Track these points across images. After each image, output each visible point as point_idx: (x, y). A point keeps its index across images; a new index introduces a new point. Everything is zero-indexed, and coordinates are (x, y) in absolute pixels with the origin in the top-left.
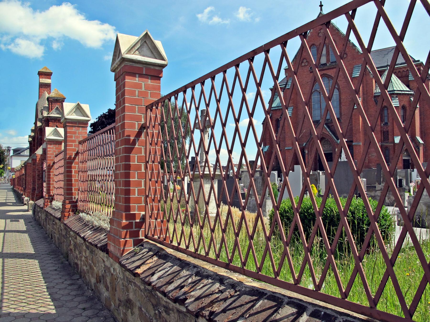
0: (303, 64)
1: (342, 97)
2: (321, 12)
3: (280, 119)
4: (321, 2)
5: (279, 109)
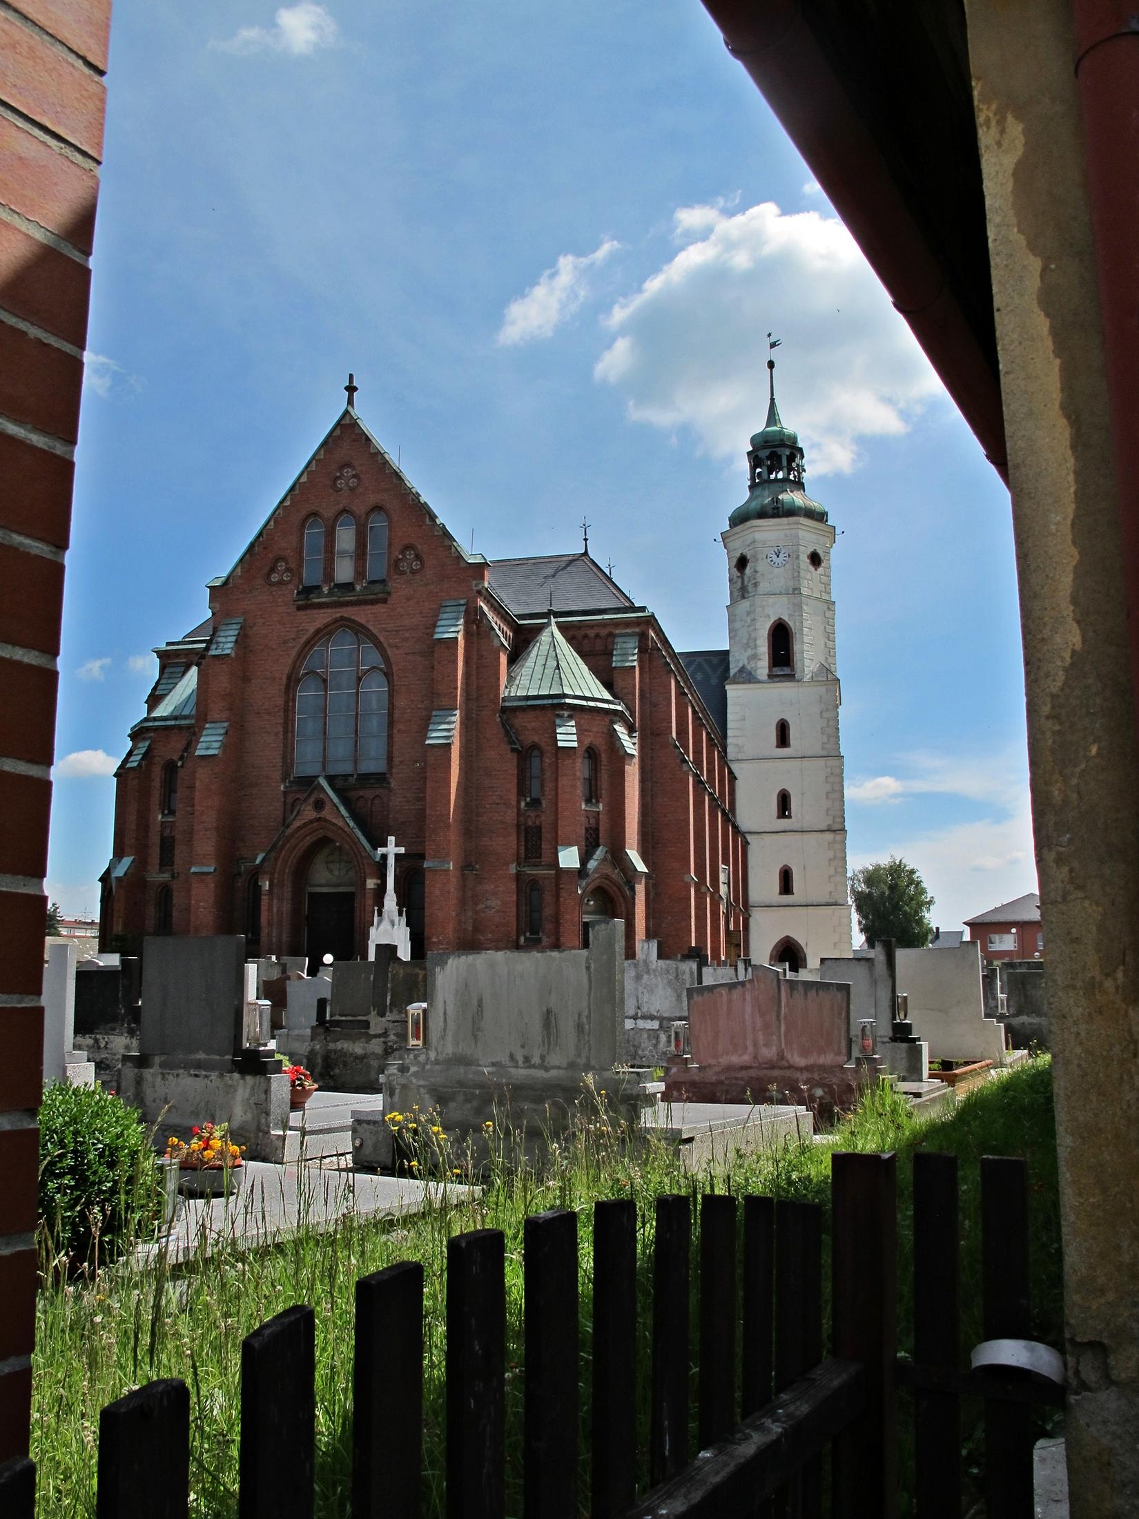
0: (275, 578)
2: (350, 409)
3: (180, 764)
4: (351, 376)
5: (180, 728)
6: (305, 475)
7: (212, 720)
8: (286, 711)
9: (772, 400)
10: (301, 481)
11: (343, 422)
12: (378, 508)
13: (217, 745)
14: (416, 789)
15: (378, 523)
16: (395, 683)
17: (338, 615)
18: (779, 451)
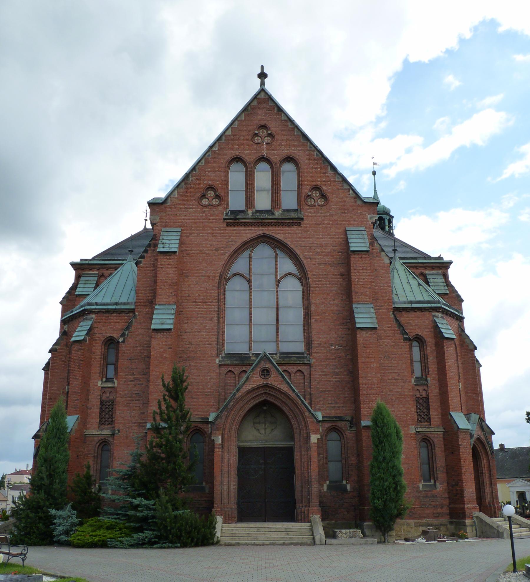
0: (205, 202)
1: (313, 301)
3: (121, 340)
4: (262, 67)
6: (230, 129)
7: (160, 303)
8: (219, 301)
9: (375, 191)
10: (227, 133)
11: (259, 97)
12: (289, 159)
13: (172, 321)
15: (288, 169)
16: (311, 285)
17: (261, 232)
18: (384, 216)
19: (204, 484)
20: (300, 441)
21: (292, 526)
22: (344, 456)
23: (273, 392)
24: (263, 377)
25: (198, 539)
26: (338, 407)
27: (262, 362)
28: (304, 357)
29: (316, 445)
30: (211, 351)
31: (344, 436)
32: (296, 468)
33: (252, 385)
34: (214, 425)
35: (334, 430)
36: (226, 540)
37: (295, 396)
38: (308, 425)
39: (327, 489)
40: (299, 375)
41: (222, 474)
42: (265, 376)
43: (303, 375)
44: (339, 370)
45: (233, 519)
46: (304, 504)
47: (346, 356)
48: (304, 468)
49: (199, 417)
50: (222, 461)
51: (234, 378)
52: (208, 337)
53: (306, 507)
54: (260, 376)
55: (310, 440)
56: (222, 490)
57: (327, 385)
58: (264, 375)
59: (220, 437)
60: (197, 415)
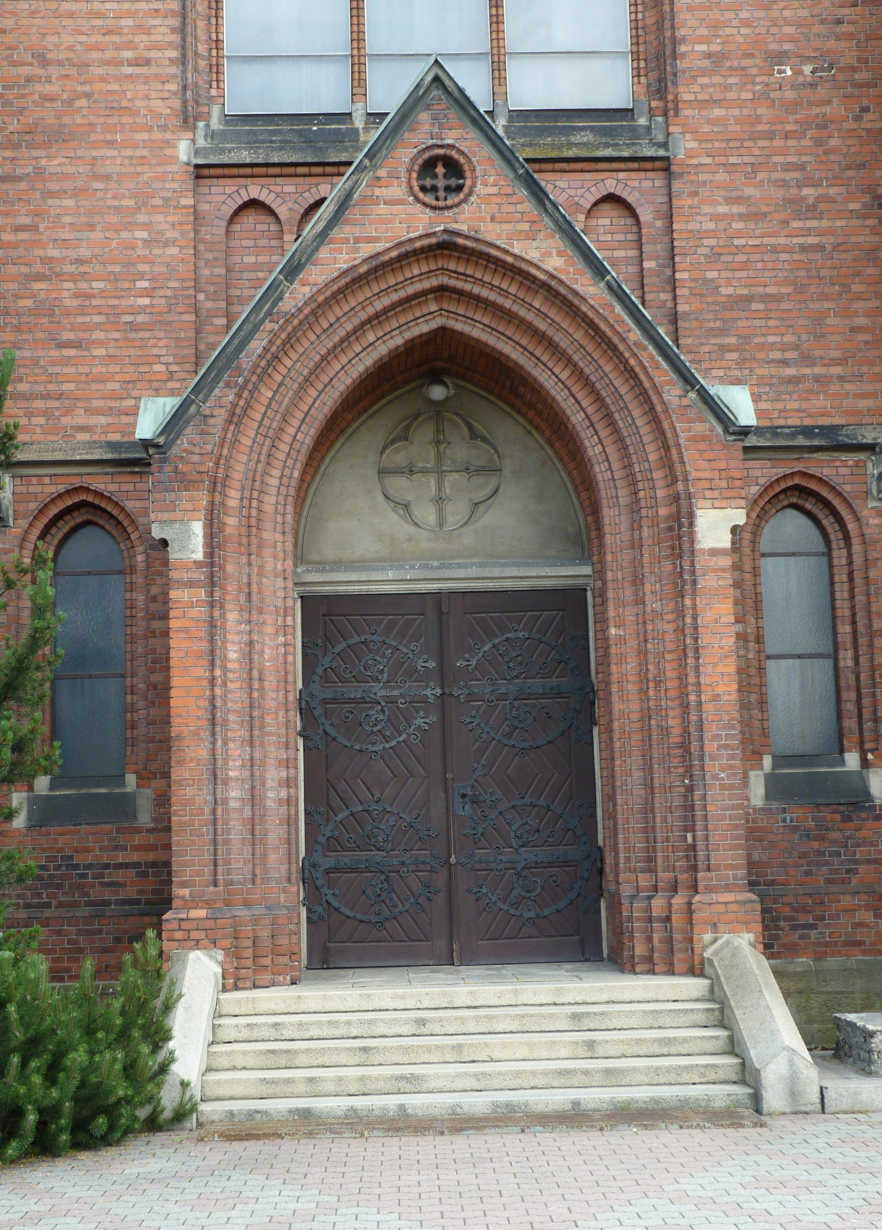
14: (788, 167)
19: (131, 779)
20: (636, 544)
21: (605, 998)
22: (848, 628)
23: (483, 284)
24: (429, 199)
25: (48, 1115)
26: (817, 379)
27: (424, 116)
28: (634, 133)
29: (726, 562)
30: (147, 97)
31: (851, 527)
32: (614, 688)
33: (371, 240)
34: (164, 461)
35: (794, 500)
36: (238, 1091)
37: (608, 297)
38: (680, 453)
39: (768, 796)
40: (607, 221)
41: (213, 722)
42: (441, 194)
43: (630, 221)
44: (821, 191)
45: (285, 960)
46: (664, 876)
47: (857, 118)
48: (658, 683)
49: (96, 438)
50: (212, 652)
51: (274, 243)
52: (129, 22)
53: (675, 891)
54: (412, 192)
55: (692, 534)
56: (214, 811)
57: (760, 266)
58: (434, 189)
59: (198, 528)
60: (83, 429)
